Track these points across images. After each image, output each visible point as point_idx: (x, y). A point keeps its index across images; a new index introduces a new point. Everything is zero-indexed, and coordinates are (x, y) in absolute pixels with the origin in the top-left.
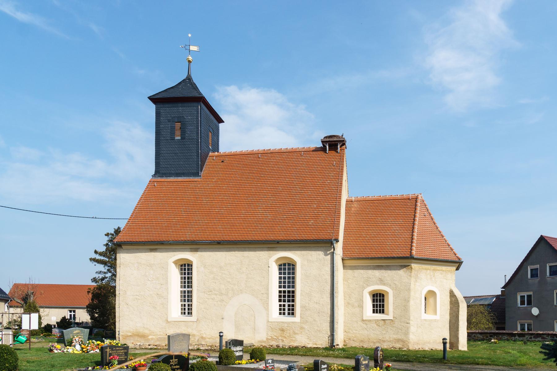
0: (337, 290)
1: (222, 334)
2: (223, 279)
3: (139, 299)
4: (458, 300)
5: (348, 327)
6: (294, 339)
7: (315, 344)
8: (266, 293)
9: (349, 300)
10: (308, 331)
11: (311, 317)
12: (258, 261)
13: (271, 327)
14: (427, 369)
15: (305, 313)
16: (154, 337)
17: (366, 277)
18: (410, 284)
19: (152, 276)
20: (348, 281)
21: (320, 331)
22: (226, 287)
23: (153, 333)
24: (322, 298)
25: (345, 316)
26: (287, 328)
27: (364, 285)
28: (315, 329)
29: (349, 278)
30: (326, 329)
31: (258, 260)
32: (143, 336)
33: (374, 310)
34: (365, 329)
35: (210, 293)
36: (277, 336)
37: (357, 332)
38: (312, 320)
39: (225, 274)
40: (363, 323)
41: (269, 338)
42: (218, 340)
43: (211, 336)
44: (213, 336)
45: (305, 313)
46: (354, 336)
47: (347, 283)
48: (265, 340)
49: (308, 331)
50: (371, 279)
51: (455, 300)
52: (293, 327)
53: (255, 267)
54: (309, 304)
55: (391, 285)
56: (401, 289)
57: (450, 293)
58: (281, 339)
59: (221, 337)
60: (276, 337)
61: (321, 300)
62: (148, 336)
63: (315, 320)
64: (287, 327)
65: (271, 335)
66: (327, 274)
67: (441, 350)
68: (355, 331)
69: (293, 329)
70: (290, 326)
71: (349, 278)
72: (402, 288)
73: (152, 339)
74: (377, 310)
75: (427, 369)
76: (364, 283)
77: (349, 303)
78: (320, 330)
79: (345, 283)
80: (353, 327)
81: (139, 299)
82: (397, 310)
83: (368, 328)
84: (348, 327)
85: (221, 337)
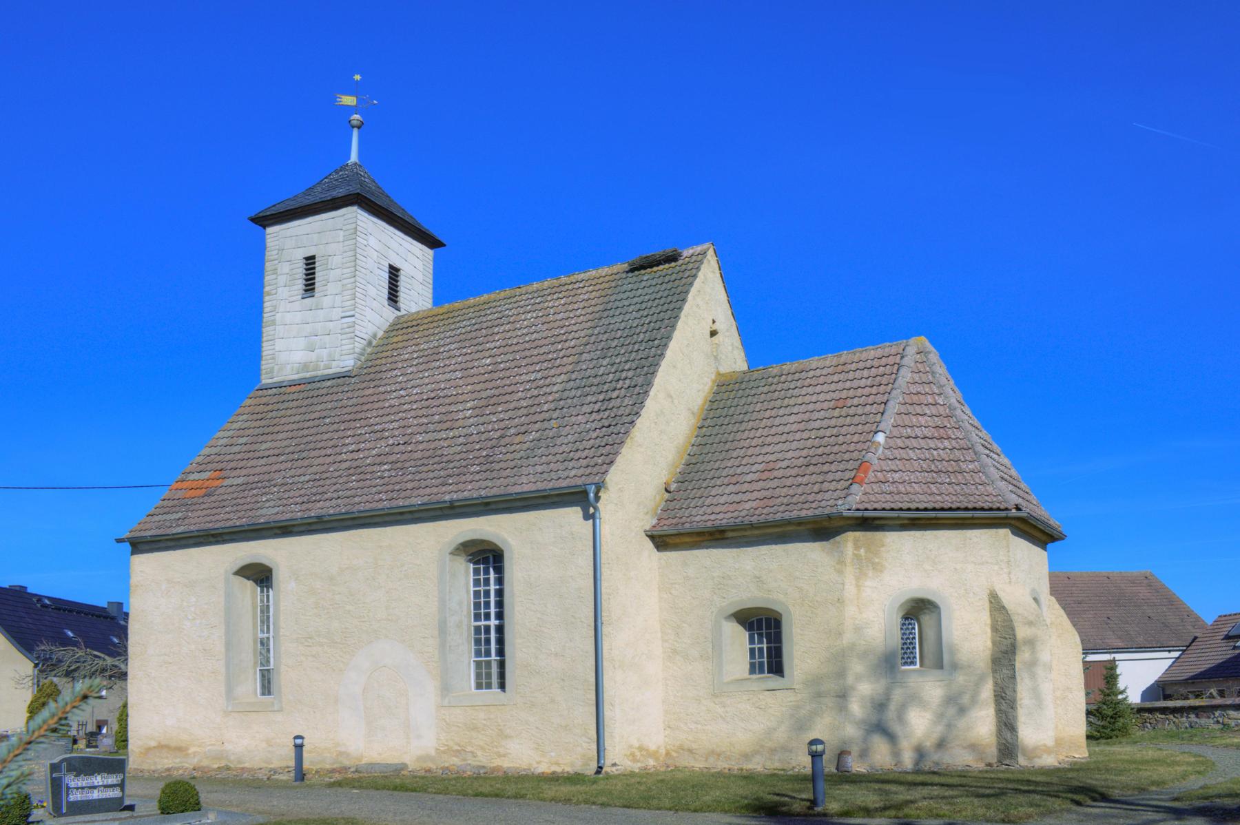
0: (607, 616)
1: (299, 741)
2: (336, 606)
3: (170, 663)
4: (1012, 621)
5: (674, 714)
6: (502, 750)
7: (556, 764)
8: (432, 637)
9: (676, 641)
10: (537, 728)
11: (544, 693)
12: (412, 555)
13: (446, 721)
14: (748, 823)
15: (528, 683)
16: (198, 749)
17: (718, 576)
18: (843, 584)
19: (193, 609)
20: (673, 592)
21: (568, 728)
22: (343, 626)
23: (198, 739)
24: (571, 641)
25: (667, 685)
26: (485, 722)
27: (715, 598)
28: (553, 723)
29: (675, 583)
30: (581, 723)
31: (412, 553)
32: (180, 750)
33: (752, 666)
34: (721, 717)
35: (308, 642)
36: (462, 744)
37: (699, 727)
38: (547, 699)
39: (340, 594)
40: (714, 702)
41: (441, 749)
42: (291, 753)
43: (313, 747)
44: (317, 745)
45: (528, 683)
46: (690, 738)
47: (670, 595)
48: (433, 753)
49: (537, 728)
50: (730, 579)
51: (1004, 621)
52: (499, 721)
53: (405, 571)
54: (537, 658)
55: (787, 594)
56: (817, 601)
57: (991, 602)
58: (472, 752)
59: (299, 747)
60: (459, 746)
61: (567, 645)
62: (187, 749)
63: (553, 701)
64: (485, 720)
65: (447, 741)
66: (582, 574)
67: (809, 775)
68: (693, 726)
69: (499, 725)
70: (492, 716)
71: (675, 583)
72: (819, 600)
73: (195, 753)
74: (761, 664)
75: (748, 823)
76: (715, 593)
77: (675, 651)
78: (566, 727)
79: (665, 596)
80: (688, 715)
81: (170, 663)
82: (808, 661)
83: (727, 715)
84: (674, 714)
85: (299, 747)
